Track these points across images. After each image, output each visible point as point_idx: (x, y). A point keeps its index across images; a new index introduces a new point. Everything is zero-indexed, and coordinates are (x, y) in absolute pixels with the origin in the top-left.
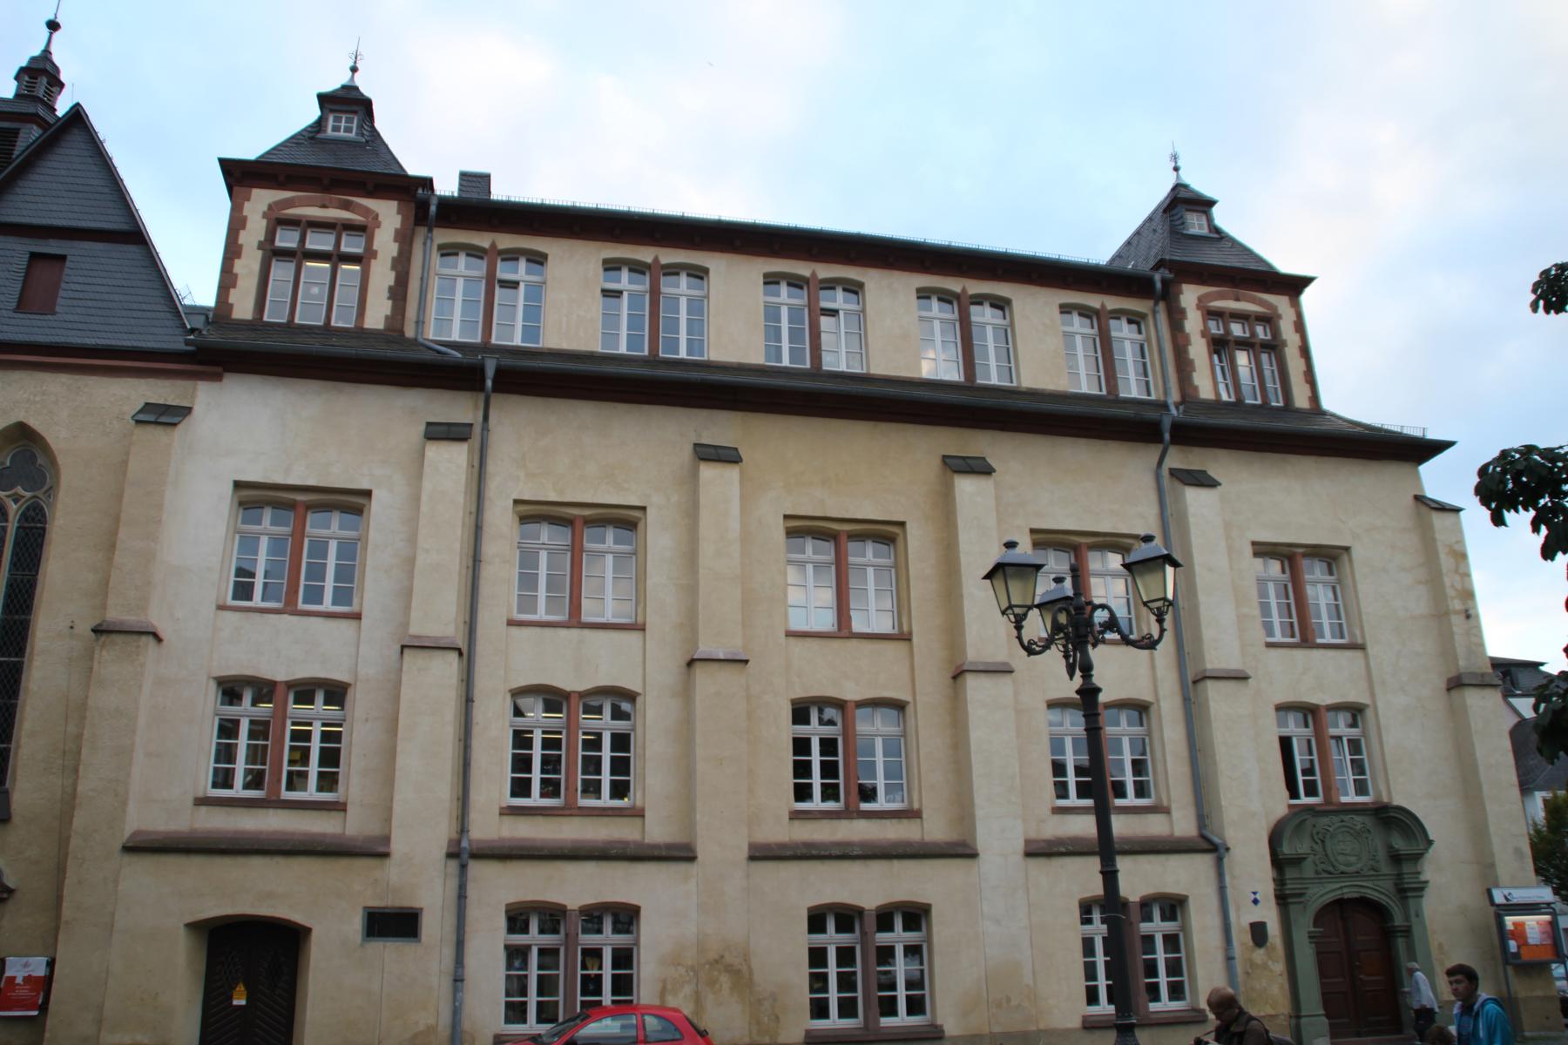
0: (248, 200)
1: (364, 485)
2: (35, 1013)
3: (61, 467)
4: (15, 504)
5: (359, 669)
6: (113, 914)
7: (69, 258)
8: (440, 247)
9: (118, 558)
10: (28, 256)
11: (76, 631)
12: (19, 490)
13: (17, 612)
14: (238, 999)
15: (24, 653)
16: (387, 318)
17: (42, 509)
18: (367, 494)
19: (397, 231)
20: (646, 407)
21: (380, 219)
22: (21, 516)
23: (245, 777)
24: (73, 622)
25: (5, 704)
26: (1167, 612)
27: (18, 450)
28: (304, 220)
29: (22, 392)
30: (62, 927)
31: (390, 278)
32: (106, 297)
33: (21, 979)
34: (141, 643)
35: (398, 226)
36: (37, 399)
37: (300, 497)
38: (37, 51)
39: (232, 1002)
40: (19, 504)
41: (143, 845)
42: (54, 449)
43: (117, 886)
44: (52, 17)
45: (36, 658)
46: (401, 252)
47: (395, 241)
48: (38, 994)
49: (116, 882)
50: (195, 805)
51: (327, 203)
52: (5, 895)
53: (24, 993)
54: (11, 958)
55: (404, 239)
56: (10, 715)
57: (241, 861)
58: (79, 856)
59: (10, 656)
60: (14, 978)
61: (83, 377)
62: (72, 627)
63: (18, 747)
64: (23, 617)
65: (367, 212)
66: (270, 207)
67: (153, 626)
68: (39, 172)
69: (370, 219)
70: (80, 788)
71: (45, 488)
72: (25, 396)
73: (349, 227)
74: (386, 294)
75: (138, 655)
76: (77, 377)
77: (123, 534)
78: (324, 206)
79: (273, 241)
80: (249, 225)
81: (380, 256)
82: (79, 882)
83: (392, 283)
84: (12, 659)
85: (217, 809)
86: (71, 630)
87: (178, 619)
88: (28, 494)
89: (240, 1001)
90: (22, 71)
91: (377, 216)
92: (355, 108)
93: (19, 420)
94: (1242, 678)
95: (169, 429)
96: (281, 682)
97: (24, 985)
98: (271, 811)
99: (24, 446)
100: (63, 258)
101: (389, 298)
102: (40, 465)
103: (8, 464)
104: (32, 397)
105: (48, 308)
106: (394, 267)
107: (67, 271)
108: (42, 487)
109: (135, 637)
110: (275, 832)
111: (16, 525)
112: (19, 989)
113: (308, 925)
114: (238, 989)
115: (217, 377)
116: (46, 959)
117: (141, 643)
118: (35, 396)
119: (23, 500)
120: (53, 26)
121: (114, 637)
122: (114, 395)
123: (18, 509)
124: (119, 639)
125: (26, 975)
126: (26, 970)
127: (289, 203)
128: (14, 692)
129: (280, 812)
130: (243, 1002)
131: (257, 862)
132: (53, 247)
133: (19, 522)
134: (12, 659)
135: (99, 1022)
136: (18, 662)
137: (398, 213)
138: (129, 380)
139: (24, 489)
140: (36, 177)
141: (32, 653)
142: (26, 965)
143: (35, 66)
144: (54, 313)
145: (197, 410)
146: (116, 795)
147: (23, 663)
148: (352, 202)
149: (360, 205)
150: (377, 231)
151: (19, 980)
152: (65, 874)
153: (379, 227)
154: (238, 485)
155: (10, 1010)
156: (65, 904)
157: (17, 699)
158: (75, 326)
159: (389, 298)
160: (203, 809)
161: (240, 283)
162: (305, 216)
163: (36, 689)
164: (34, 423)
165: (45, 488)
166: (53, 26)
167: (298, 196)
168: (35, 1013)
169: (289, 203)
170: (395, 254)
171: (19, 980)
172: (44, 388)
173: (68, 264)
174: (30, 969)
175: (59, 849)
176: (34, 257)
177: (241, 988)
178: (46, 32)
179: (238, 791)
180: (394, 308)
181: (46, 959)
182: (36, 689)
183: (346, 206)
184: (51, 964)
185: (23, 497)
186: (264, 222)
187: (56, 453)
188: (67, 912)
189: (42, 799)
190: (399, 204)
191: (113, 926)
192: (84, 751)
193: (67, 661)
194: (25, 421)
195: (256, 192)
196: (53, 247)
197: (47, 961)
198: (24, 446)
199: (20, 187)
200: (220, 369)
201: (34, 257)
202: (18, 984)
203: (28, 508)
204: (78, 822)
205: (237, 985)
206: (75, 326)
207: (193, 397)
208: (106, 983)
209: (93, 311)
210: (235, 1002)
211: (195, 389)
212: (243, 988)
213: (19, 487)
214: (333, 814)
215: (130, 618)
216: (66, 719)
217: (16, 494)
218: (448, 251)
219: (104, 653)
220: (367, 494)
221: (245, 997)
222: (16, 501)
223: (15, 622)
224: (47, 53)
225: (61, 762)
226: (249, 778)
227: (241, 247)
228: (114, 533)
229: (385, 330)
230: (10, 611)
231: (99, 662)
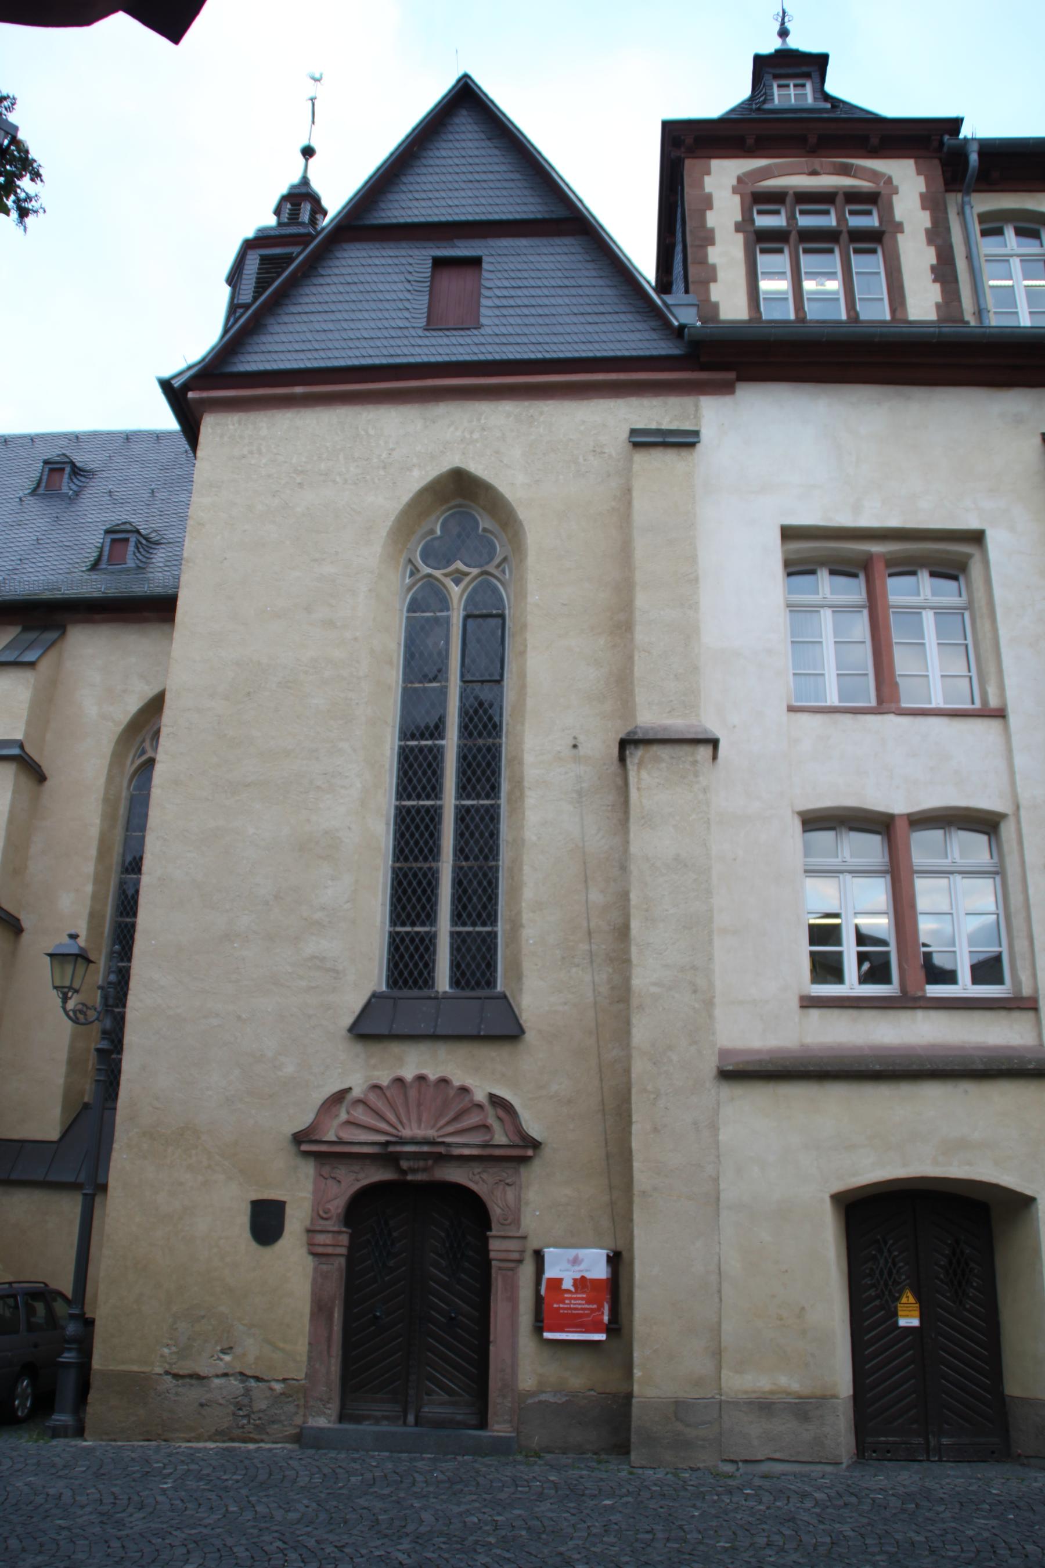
0: (709, 173)
1: (972, 523)
2: (602, 1337)
3: (525, 523)
4: (457, 585)
5: (1019, 790)
6: (716, 1180)
7: (485, 259)
8: (983, 218)
9: (641, 635)
10: (431, 261)
11: (582, 751)
12: (459, 565)
13: (480, 735)
14: (907, 1316)
15: (499, 792)
16: (938, 306)
17: (495, 590)
18: (977, 538)
19: (922, 196)
20: (919, 393)
21: (895, 182)
22: (467, 601)
23: (860, 964)
24: (575, 738)
25: (480, 868)
26: (70, 998)
27: (451, 512)
28: (791, 192)
29: (452, 429)
30: (637, 1200)
31: (929, 256)
32: (546, 301)
33: (571, 1282)
34: (699, 758)
35: (923, 190)
36: (476, 436)
37: (876, 548)
38: (296, 179)
39: (897, 1322)
40: (462, 585)
41: (750, 1068)
42: (510, 499)
43: (717, 1135)
44: (304, 143)
45: (528, 793)
46: (935, 221)
47: (924, 208)
48: (600, 1307)
49: (714, 1128)
50: (802, 1007)
51: (818, 168)
52: (530, 1153)
53: (578, 1303)
54: (552, 1249)
55: (932, 203)
56: (490, 883)
57: (906, 1090)
58: (650, 1087)
59: (478, 797)
60: (559, 1281)
61: (536, 402)
62: (575, 746)
63: (516, 926)
64: (490, 741)
65: (874, 175)
66: (740, 180)
67: (706, 731)
68: (446, 138)
69: (882, 184)
70: (636, 982)
71: (497, 560)
72: (459, 433)
73: (853, 197)
74: (930, 277)
75: (696, 776)
76: (526, 403)
77: (641, 600)
78: (814, 173)
79: (753, 221)
80: (716, 203)
81: (907, 228)
82: (655, 1130)
83: (934, 261)
84: (482, 802)
85: (836, 1012)
86: (575, 751)
87: (734, 727)
88: (475, 571)
89: (909, 1320)
90: (284, 199)
91: (889, 180)
92: (805, 69)
93: (455, 465)
94: (967, 914)
95: (684, 452)
96: (901, 816)
97: (576, 1292)
98: (920, 1014)
99: (460, 506)
100: (476, 262)
101: (935, 281)
102: (485, 530)
103: (439, 532)
104: (467, 436)
105: (470, 322)
106: (930, 241)
107: (485, 274)
108: (491, 559)
109: (687, 749)
110: (933, 1047)
111: (462, 613)
112: (570, 1299)
113: (1028, 1192)
114: (904, 1300)
115: (726, 388)
116: (605, 1252)
117: (699, 758)
118: (472, 433)
119: (467, 579)
120: (308, 152)
121: (655, 749)
122: (584, 422)
123: (464, 591)
124: (664, 752)
125: (578, 1276)
126: (577, 1268)
127: (765, 173)
128: (491, 850)
129: (934, 1015)
130: (915, 1322)
131: (933, 1092)
132: (462, 249)
133: (465, 609)
134: (482, 802)
135: (717, 1354)
136: (492, 806)
137: (919, 173)
138: (601, 401)
139: (466, 564)
140: (411, 179)
141: (518, 784)
142: (575, 1261)
143: (297, 191)
144: (479, 326)
145: (707, 434)
146: (695, 992)
147: (499, 806)
148: (852, 165)
149: (865, 169)
150: (895, 199)
151: (568, 1285)
152: (630, 1116)
153: (897, 193)
154: (789, 534)
155: (561, 1330)
156: (636, 1165)
157: (497, 860)
158: (511, 340)
159: (935, 281)
160: (815, 1014)
161: (721, 274)
162: (791, 187)
163: (534, 838)
164: (477, 468)
165: (497, 560)
166: (308, 152)
167: (775, 165)
168: (602, 1337)
169: (765, 173)
170: (928, 224)
171: (568, 1285)
172: (483, 421)
173: (485, 266)
174: (582, 1267)
175: (601, 1080)
176: (439, 263)
177: (908, 1298)
178: (301, 160)
179: (851, 985)
180: (944, 292)
181: (605, 1252)
182: (534, 838)
183: (845, 171)
184: (615, 1260)
185: (467, 574)
186: (737, 199)
187: (514, 504)
188: (642, 1177)
189: (565, 1004)
190: (916, 163)
191: (718, 1199)
192: (635, 925)
193: (575, 795)
194: (463, 466)
195: (716, 164)
196: (462, 249)
197: (608, 1256)
198: (460, 506)
199: (425, 158)
200: (732, 375)
201: (439, 263)
202: (568, 1291)
203: (475, 590)
204: (641, 1033)
205: (901, 1292)
206: (511, 340)
207: (697, 416)
208: (719, 1292)
209: (532, 320)
210: (903, 1322)
211: (697, 407)
212: (912, 1300)
213: (459, 562)
214: (1016, 1014)
215: (677, 723)
216: (586, 881)
217: (457, 571)
218: (992, 226)
219: (644, 774)
220: (977, 538)
221: (917, 1313)
222: (457, 582)
223: (479, 750)
224: (305, 181)
225: (587, 947)
226: (866, 966)
227: (712, 231)
228: (626, 606)
229: (939, 321)
230: (471, 734)
231: (638, 789)
